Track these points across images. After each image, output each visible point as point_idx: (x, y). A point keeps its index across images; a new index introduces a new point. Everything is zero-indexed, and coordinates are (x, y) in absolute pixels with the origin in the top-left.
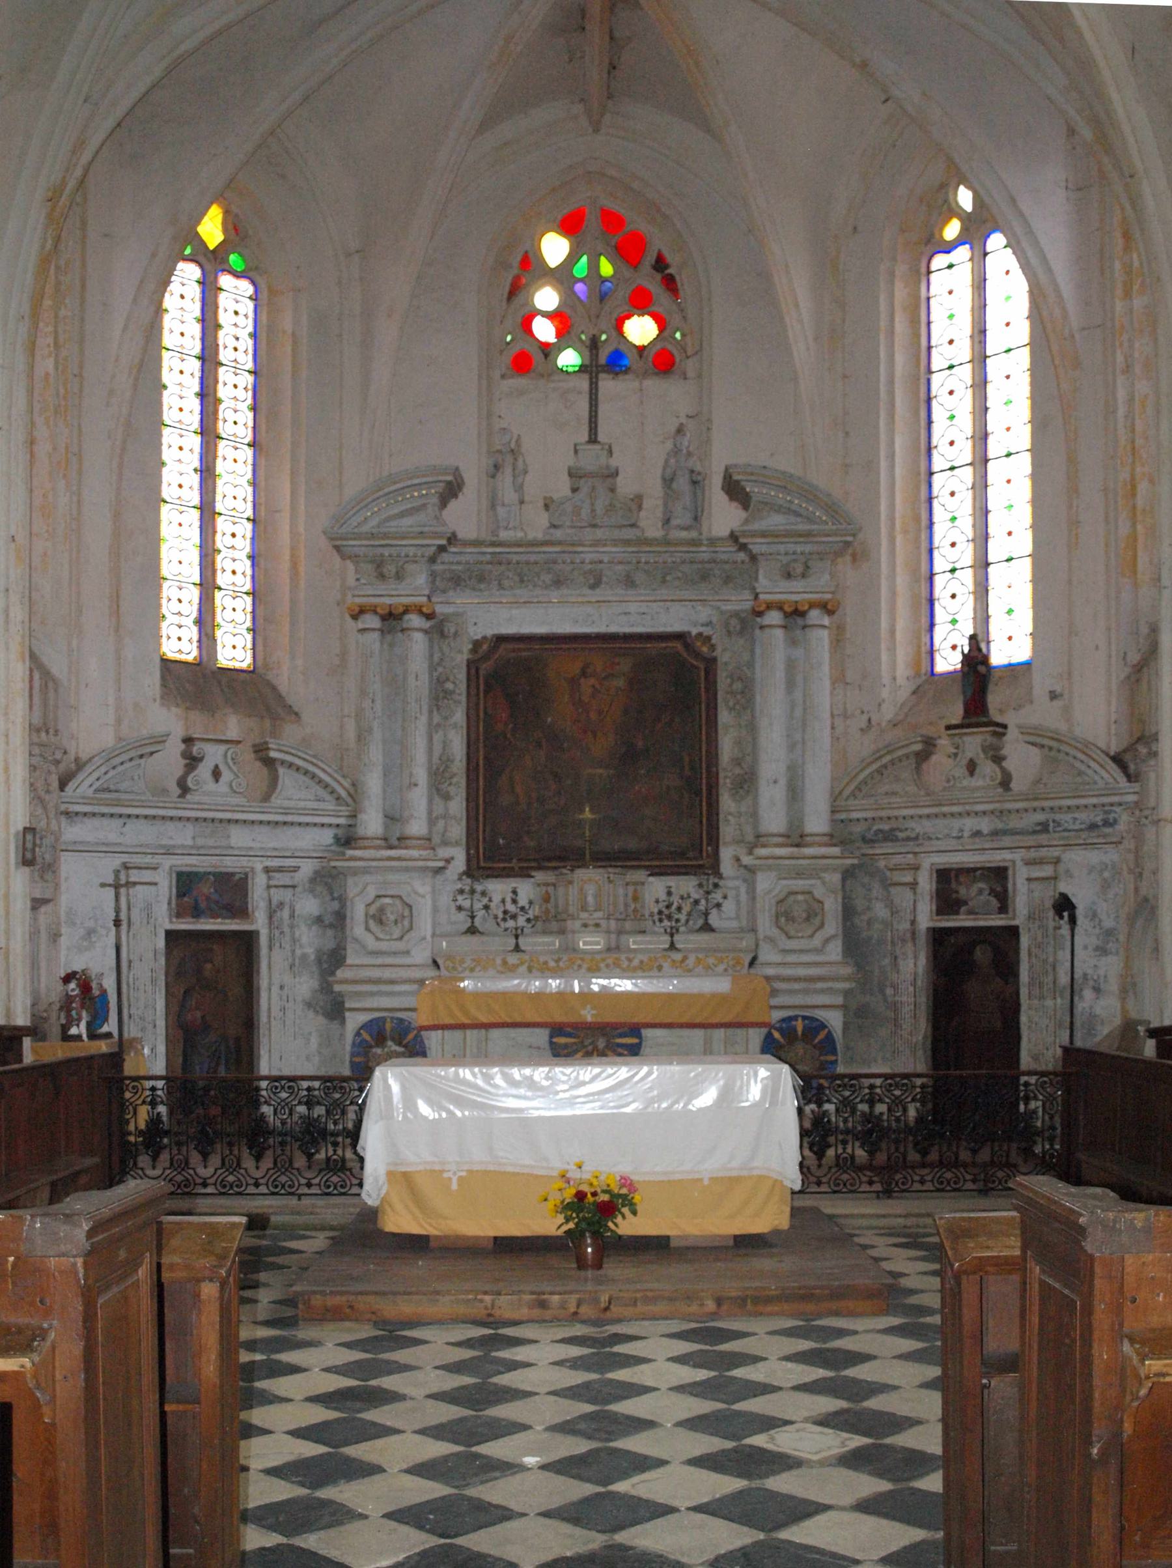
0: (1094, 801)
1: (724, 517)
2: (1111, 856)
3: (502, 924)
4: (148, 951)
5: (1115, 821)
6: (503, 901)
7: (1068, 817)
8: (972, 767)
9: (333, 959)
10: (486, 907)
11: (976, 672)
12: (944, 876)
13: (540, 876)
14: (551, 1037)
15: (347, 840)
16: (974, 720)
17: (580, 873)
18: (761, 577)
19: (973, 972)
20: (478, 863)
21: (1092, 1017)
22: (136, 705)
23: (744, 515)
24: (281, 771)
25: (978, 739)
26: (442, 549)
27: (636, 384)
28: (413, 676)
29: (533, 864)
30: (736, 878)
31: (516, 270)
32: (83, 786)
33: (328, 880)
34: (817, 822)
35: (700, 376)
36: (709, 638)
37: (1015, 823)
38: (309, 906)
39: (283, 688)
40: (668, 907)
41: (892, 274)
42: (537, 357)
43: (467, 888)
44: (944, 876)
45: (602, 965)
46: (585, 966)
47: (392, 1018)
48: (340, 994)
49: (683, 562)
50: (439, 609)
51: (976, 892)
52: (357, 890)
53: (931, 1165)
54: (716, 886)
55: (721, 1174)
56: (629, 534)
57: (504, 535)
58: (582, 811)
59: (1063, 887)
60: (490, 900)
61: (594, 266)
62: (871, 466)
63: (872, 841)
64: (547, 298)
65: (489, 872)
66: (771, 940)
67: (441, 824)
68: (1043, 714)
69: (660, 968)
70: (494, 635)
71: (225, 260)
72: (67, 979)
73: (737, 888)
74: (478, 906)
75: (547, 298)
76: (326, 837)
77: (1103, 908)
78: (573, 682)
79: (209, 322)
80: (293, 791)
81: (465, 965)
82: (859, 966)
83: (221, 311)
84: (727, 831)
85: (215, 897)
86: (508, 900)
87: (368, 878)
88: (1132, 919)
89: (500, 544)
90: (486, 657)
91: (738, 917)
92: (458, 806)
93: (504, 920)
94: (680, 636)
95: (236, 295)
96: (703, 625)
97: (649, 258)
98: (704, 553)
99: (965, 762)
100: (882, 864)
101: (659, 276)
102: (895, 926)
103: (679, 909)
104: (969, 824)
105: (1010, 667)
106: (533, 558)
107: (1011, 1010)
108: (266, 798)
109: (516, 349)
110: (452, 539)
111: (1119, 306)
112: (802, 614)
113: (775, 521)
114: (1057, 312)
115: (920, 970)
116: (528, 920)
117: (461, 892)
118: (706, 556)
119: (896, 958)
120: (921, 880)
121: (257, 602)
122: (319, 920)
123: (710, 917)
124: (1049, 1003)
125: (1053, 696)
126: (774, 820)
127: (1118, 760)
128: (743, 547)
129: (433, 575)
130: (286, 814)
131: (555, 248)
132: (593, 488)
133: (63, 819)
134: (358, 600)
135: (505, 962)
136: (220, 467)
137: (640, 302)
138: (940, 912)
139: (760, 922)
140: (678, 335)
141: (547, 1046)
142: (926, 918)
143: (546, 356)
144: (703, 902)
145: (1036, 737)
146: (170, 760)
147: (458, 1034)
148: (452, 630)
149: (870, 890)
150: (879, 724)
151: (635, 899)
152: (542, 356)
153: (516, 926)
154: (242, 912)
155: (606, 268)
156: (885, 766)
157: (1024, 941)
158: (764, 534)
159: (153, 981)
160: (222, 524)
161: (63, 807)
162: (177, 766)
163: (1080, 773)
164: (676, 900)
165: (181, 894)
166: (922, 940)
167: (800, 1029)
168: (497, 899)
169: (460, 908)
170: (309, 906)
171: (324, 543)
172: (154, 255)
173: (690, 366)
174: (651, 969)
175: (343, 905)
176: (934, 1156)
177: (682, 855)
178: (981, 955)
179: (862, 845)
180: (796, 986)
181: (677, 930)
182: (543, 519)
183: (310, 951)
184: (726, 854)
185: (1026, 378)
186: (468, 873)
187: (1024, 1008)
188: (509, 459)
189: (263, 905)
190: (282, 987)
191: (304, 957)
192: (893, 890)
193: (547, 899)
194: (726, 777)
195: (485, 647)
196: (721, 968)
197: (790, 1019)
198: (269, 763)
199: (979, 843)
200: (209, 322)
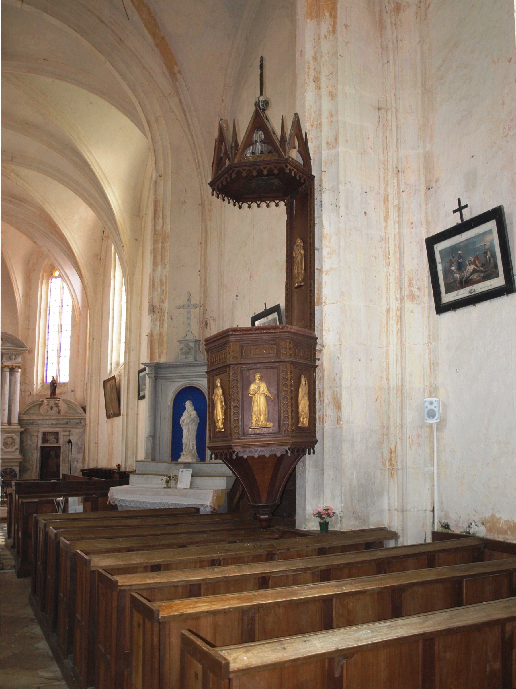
8: (52, 408)
12: (44, 434)
21: (76, 468)
34: (15, 419)
37: (61, 422)
44: (44, 434)
51: (51, 438)
62: (34, 330)
68: (70, 397)
104: (51, 422)
107: (58, 466)
112: (14, 369)
125: (72, 391)
138: (43, 442)
145: (66, 402)
157: (62, 450)
163: (76, 411)
166: (39, 448)
178: (52, 453)
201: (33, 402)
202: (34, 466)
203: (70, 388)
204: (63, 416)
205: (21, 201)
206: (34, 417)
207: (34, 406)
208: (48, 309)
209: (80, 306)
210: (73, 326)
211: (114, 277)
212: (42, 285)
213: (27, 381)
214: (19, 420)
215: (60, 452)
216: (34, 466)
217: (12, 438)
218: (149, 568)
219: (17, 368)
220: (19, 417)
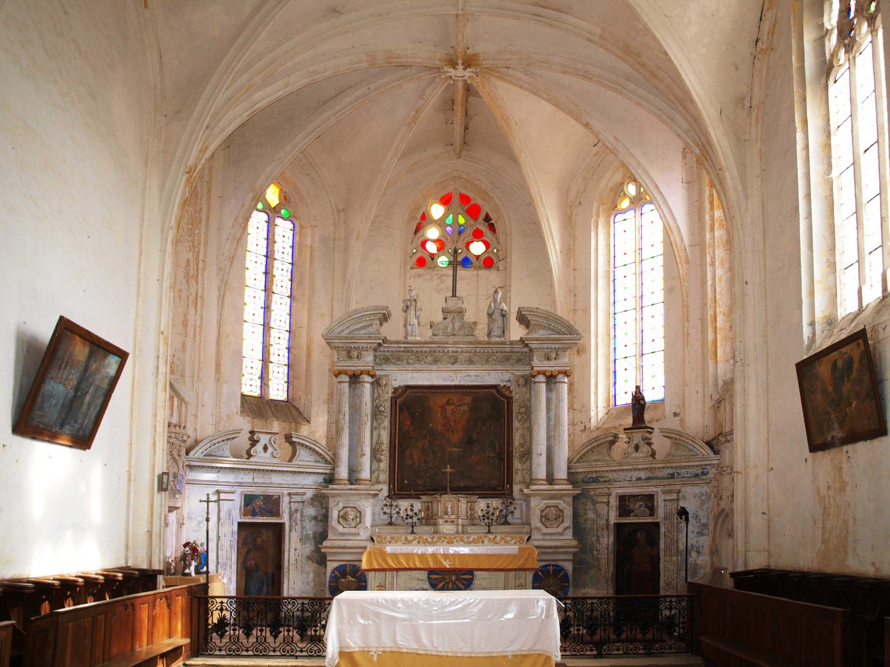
0: (697, 463)
1: (516, 332)
2: (706, 489)
4: (230, 531)
5: (707, 473)
7: (684, 471)
8: (637, 448)
9: (322, 536)
10: (398, 513)
11: (639, 403)
12: (622, 499)
13: (424, 498)
15: (330, 480)
16: (638, 425)
17: (445, 497)
18: (535, 359)
19: (637, 543)
21: (696, 565)
22: (228, 416)
23: (526, 331)
24: (298, 447)
25: (640, 435)
26: (380, 345)
27: (475, 272)
32: (197, 453)
33: (320, 500)
34: (561, 473)
35: (505, 269)
36: (509, 387)
37: (658, 474)
38: (311, 511)
41: (597, 223)
42: (428, 259)
44: (622, 499)
48: (324, 553)
50: (378, 373)
51: (638, 506)
52: (334, 504)
53: (622, 641)
54: (511, 503)
55: (518, 653)
56: (471, 339)
57: (410, 338)
59: (682, 504)
61: (456, 219)
62: (587, 310)
63: (587, 482)
64: (433, 233)
66: (537, 529)
67: (376, 473)
68: (673, 424)
69: (483, 542)
71: (279, 212)
72: (185, 546)
73: (521, 504)
74: (394, 512)
75: (433, 233)
76: (320, 479)
77: (701, 514)
78: (443, 408)
79: (270, 239)
80: (304, 458)
83: (276, 236)
84: (517, 478)
85: (264, 507)
86: (409, 510)
87: (339, 499)
88: (716, 518)
89: (408, 343)
91: (521, 518)
92: (384, 465)
94: (495, 387)
95: (284, 228)
97: (482, 216)
98: (507, 348)
99: (633, 445)
100: (592, 493)
101: (486, 224)
103: (493, 514)
104: (635, 474)
105: (654, 403)
106: (424, 350)
107: (655, 561)
108: (290, 460)
109: (419, 255)
110: (385, 341)
111: (708, 235)
112: (555, 377)
113: (541, 333)
114: (678, 238)
115: (611, 543)
117: (386, 505)
118: (508, 350)
120: (611, 500)
122: (315, 518)
124: (674, 558)
125: (675, 415)
126: (541, 472)
127: (709, 444)
128: (526, 345)
129: (375, 356)
131: (437, 211)
133: (188, 469)
135: (406, 539)
136: (273, 306)
137: (478, 235)
138: (620, 516)
139: (532, 520)
142: (613, 518)
143: (432, 259)
145: (667, 434)
146: (243, 441)
147: (383, 574)
151: (471, 509)
153: (412, 525)
154: (277, 514)
155: (461, 220)
156: (594, 448)
157: (662, 529)
159: (231, 547)
160: (273, 333)
161: (187, 463)
162: (247, 444)
163: (690, 450)
164: (491, 510)
165: (246, 505)
166: (612, 527)
168: (403, 509)
169: (385, 513)
170: (311, 511)
171: (324, 342)
172: (243, 206)
175: (327, 511)
176: (624, 636)
177: (495, 489)
179: (583, 485)
180: (550, 550)
182: (429, 333)
183: (310, 532)
184: (516, 488)
185: (661, 270)
186: (389, 496)
187: (662, 561)
188: (413, 303)
189: (287, 511)
191: (307, 535)
192: (598, 505)
193: (428, 509)
196: (514, 541)
197: (546, 566)
198: (292, 443)
199: (640, 483)
200: (270, 239)
201: (590, 442)
202: (603, 562)
203: (669, 410)
204: (664, 462)
205: (560, 11)
206: (600, 467)
208: (612, 269)
209: (687, 245)
210: (669, 290)
211: (805, 122)
212: (597, 227)
213: (579, 405)
214: (569, 473)
215: (659, 534)
216: (603, 562)
219: (560, 376)
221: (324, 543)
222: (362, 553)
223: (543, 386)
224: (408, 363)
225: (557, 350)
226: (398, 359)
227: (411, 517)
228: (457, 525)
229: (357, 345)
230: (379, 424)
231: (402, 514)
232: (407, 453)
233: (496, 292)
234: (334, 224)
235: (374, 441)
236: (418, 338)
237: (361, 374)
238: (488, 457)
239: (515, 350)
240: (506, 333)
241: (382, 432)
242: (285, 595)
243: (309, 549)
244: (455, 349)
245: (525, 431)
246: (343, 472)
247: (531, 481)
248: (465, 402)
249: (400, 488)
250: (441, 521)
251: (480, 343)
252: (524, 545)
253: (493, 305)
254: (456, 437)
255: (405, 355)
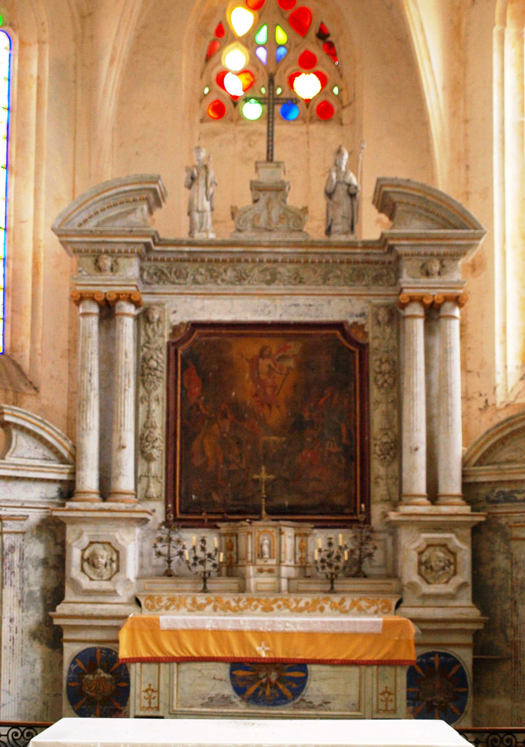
3: (193, 568)
6: (194, 548)
9: (54, 595)
10: (181, 554)
13: (224, 527)
14: (232, 670)
15: (69, 491)
20: (175, 515)
24: (14, 433)
27: (304, 128)
28: (123, 353)
29: (219, 517)
30: (384, 532)
31: (212, 36)
33: (53, 529)
34: (452, 484)
35: (352, 122)
36: (363, 326)
39: (26, 366)
40: (329, 556)
41: (502, 36)
43: (165, 537)
45: (274, 606)
46: (261, 606)
47: (102, 649)
49: (342, 262)
50: (146, 299)
54: (368, 538)
57: (198, 236)
58: (259, 472)
60: (184, 548)
62: (487, 193)
65: (184, 523)
66: (413, 586)
67: (144, 481)
69: (322, 609)
70: (189, 322)
73: (385, 540)
74: (174, 552)
75: (234, 58)
76: (53, 490)
78: (254, 363)
81: (162, 604)
82: (484, 611)
84: (378, 491)
86: (198, 548)
90: (182, 341)
91: (385, 566)
92: (157, 467)
93: (195, 564)
94: (339, 326)
96: (357, 316)
97: (313, 30)
98: (359, 254)
101: (321, 43)
102: (514, 575)
103: (338, 558)
106: (221, 257)
109: (213, 98)
110: (158, 241)
113: (415, 227)
116: (214, 566)
117: (160, 540)
118: (360, 258)
119: (515, 603)
121: (6, 295)
123: (363, 565)
126: (418, 482)
128: (391, 249)
129: (142, 269)
130: (18, 470)
131: (241, 20)
132: (270, 200)
134: (79, 288)
135: (194, 602)
137: (307, 62)
140: (336, 91)
141: (228, 678)
144: (358, 552)
147: (154, 667)
148: (156, 316)
149: (493, 544)
150: (494, 405)
151: (303, 548)
152: (232, 105)
155: (281, 36)
158: (407, 237)
164: (335, 549)
167: (437, 664)
168: (189, 546)
173: (346, 115)
174: (314, 611)
175: (64, 551)
177: (342, 513)
181: (336, 576)
183: (36, 589)
184: (377, 510)
186: (166, 523)
188: (203, 172)
190: (11, 620)
191: (31, 593)
194: (375, 445)
195: (182, 331)
196: (374, 608)
201: (500, 426)
207: (513, 434)
217: (444, 546)
218: (59, 455)
219: (448, 305)
220: (464, 475)
221: (58, 607)
222: (118, 628)
223: (419, 325)
224: (195, 282)
225: (441, 258)
226: (179, 274)
227: (202, 562)
228: (279, 577)
229: (109, 248)
230: (149, 392)
231: (187, 555)
232: (196, 444)
233: (339, 152)
234: (75, 40)
235: (141, 422)
236: (212, 236)
237: (118, 299)
238: (330, 454)
239: (372, 258)
240: (356, 227)
241: (154, 406)
242: (162, 628)
243: (33, 617)
244: (272, 257)
245: (390, 407)
246: (89, 479)
247: (398, 497)
248: (289, 352)
249: (187, 507)
250: (251, 570)
251: (313, 244)
252: (391, 618)
253: (334, 175)
254: (275, 416)
255: (191, 268)
